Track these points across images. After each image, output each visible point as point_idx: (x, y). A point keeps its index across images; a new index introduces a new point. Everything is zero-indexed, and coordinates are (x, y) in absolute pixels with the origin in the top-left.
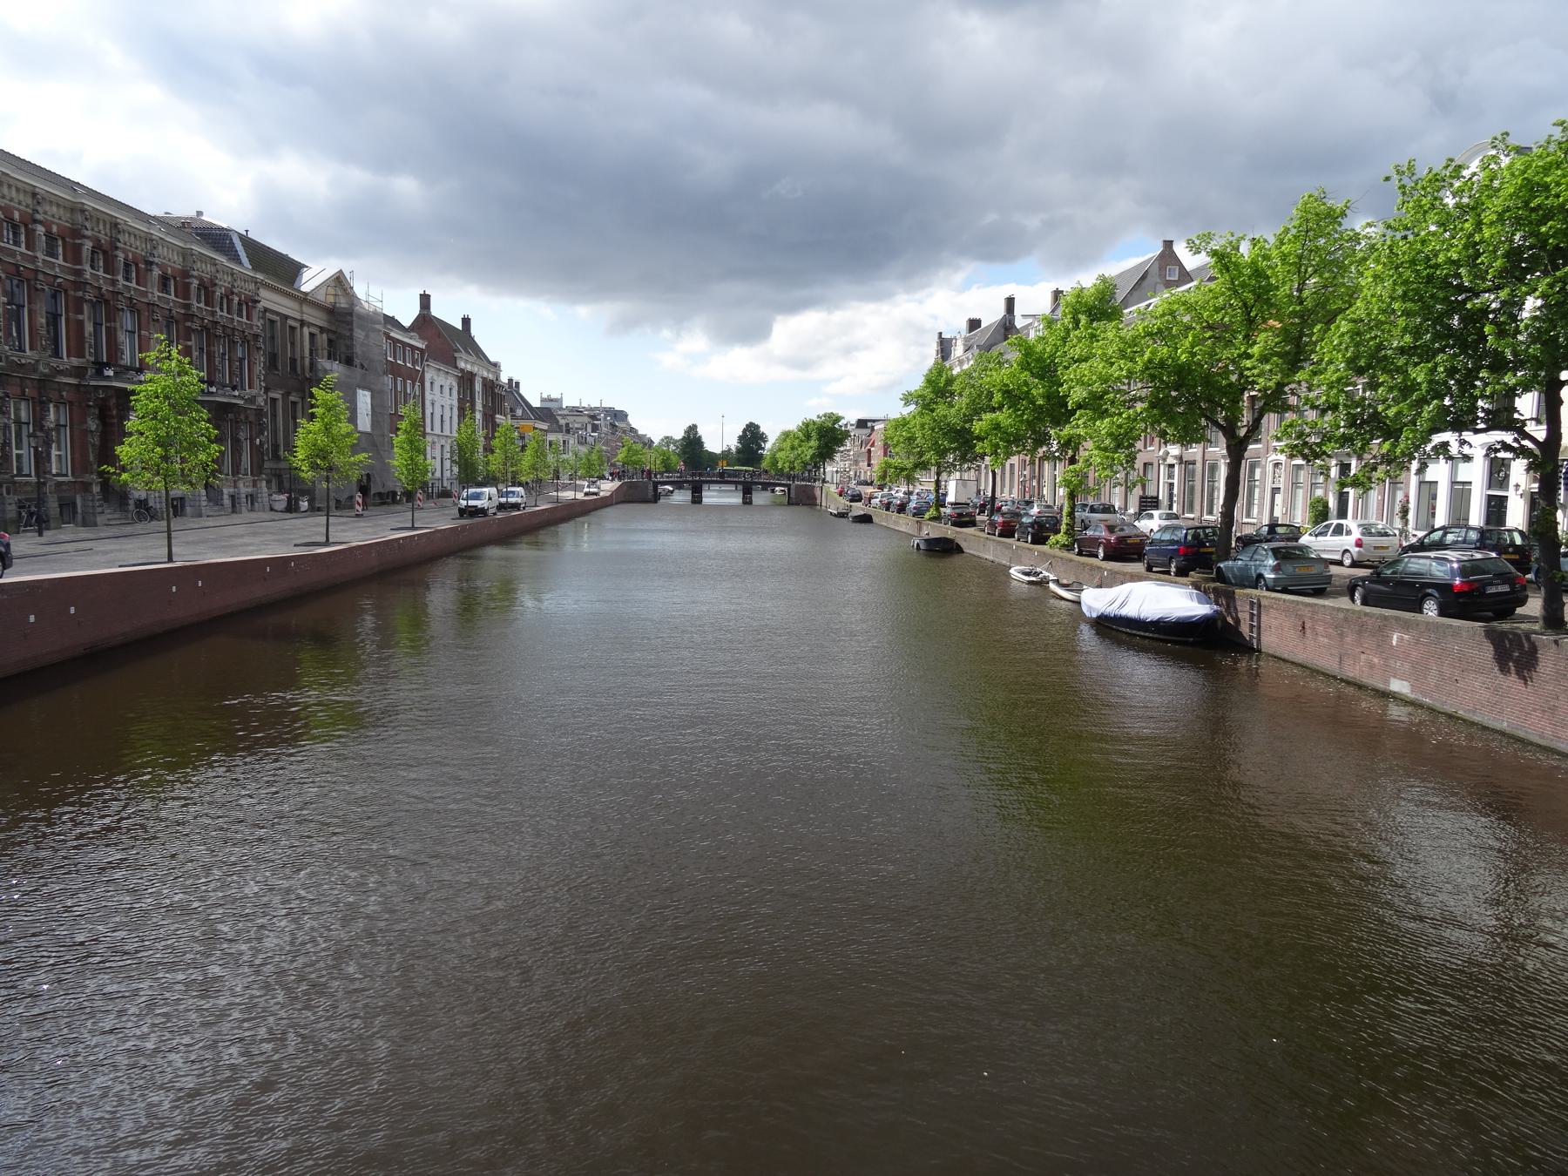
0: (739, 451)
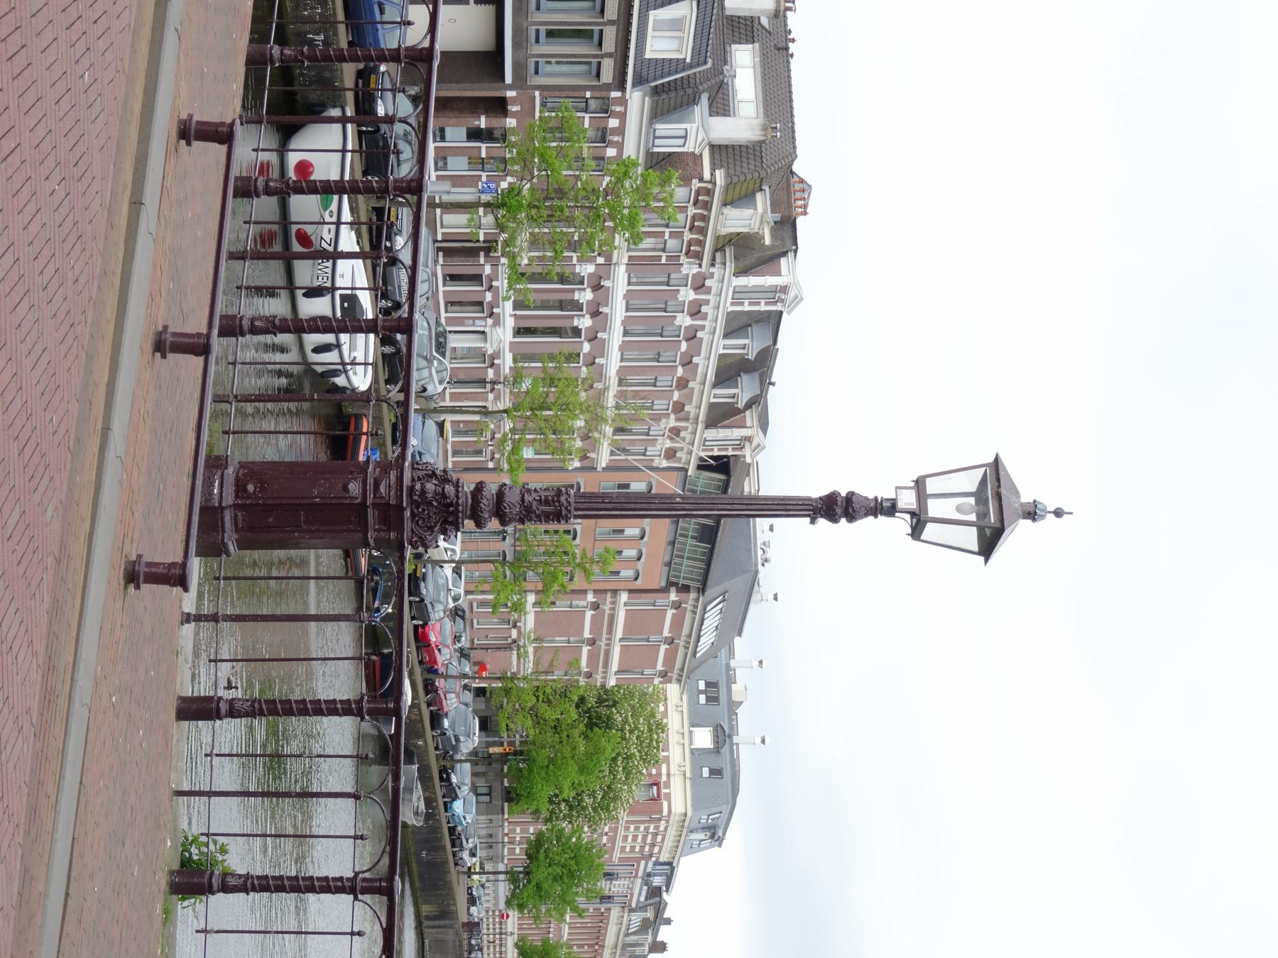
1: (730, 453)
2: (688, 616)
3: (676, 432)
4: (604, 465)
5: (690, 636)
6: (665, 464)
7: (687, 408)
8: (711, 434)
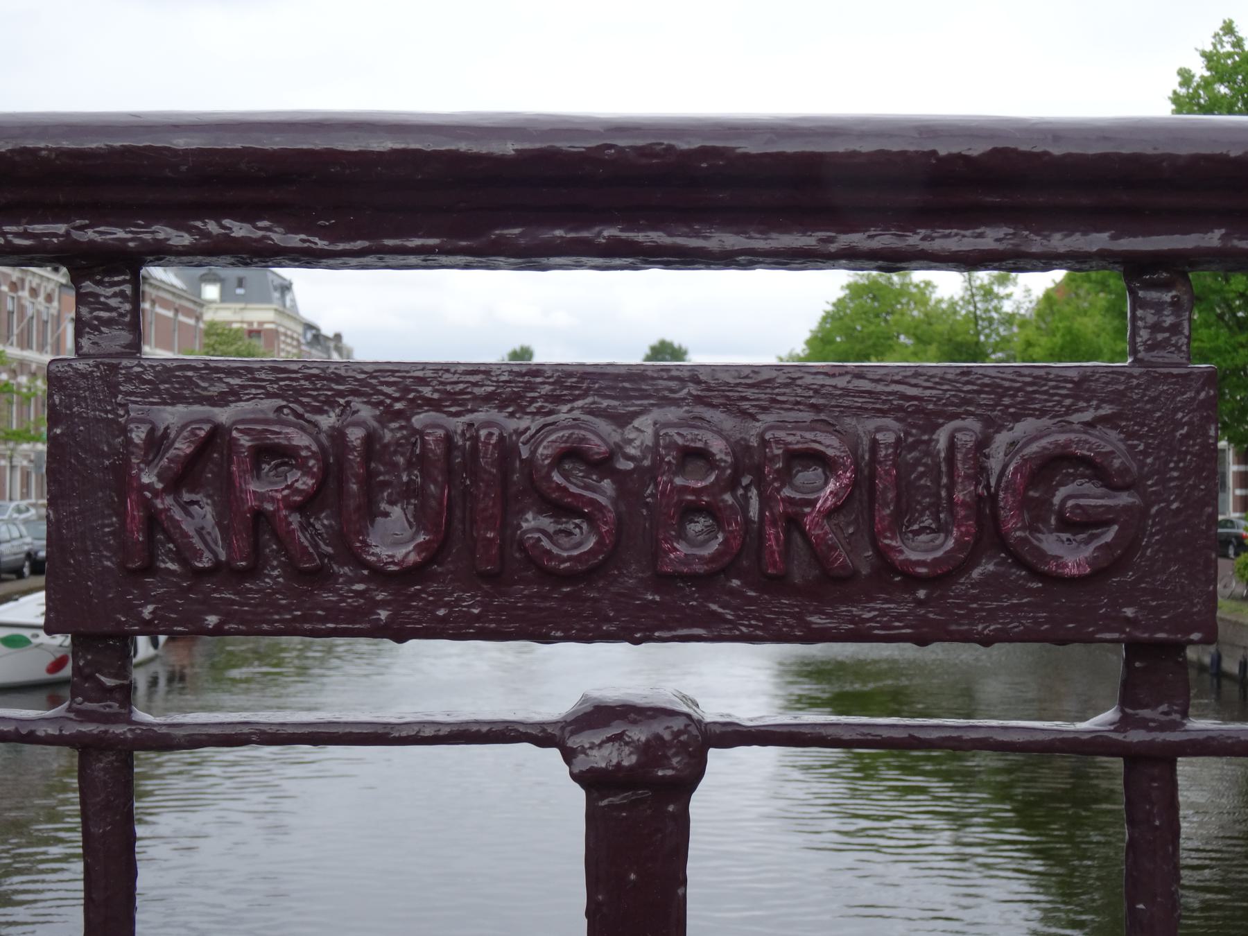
3: (34, 292)
5: (174, 294)
7: (14, 279)
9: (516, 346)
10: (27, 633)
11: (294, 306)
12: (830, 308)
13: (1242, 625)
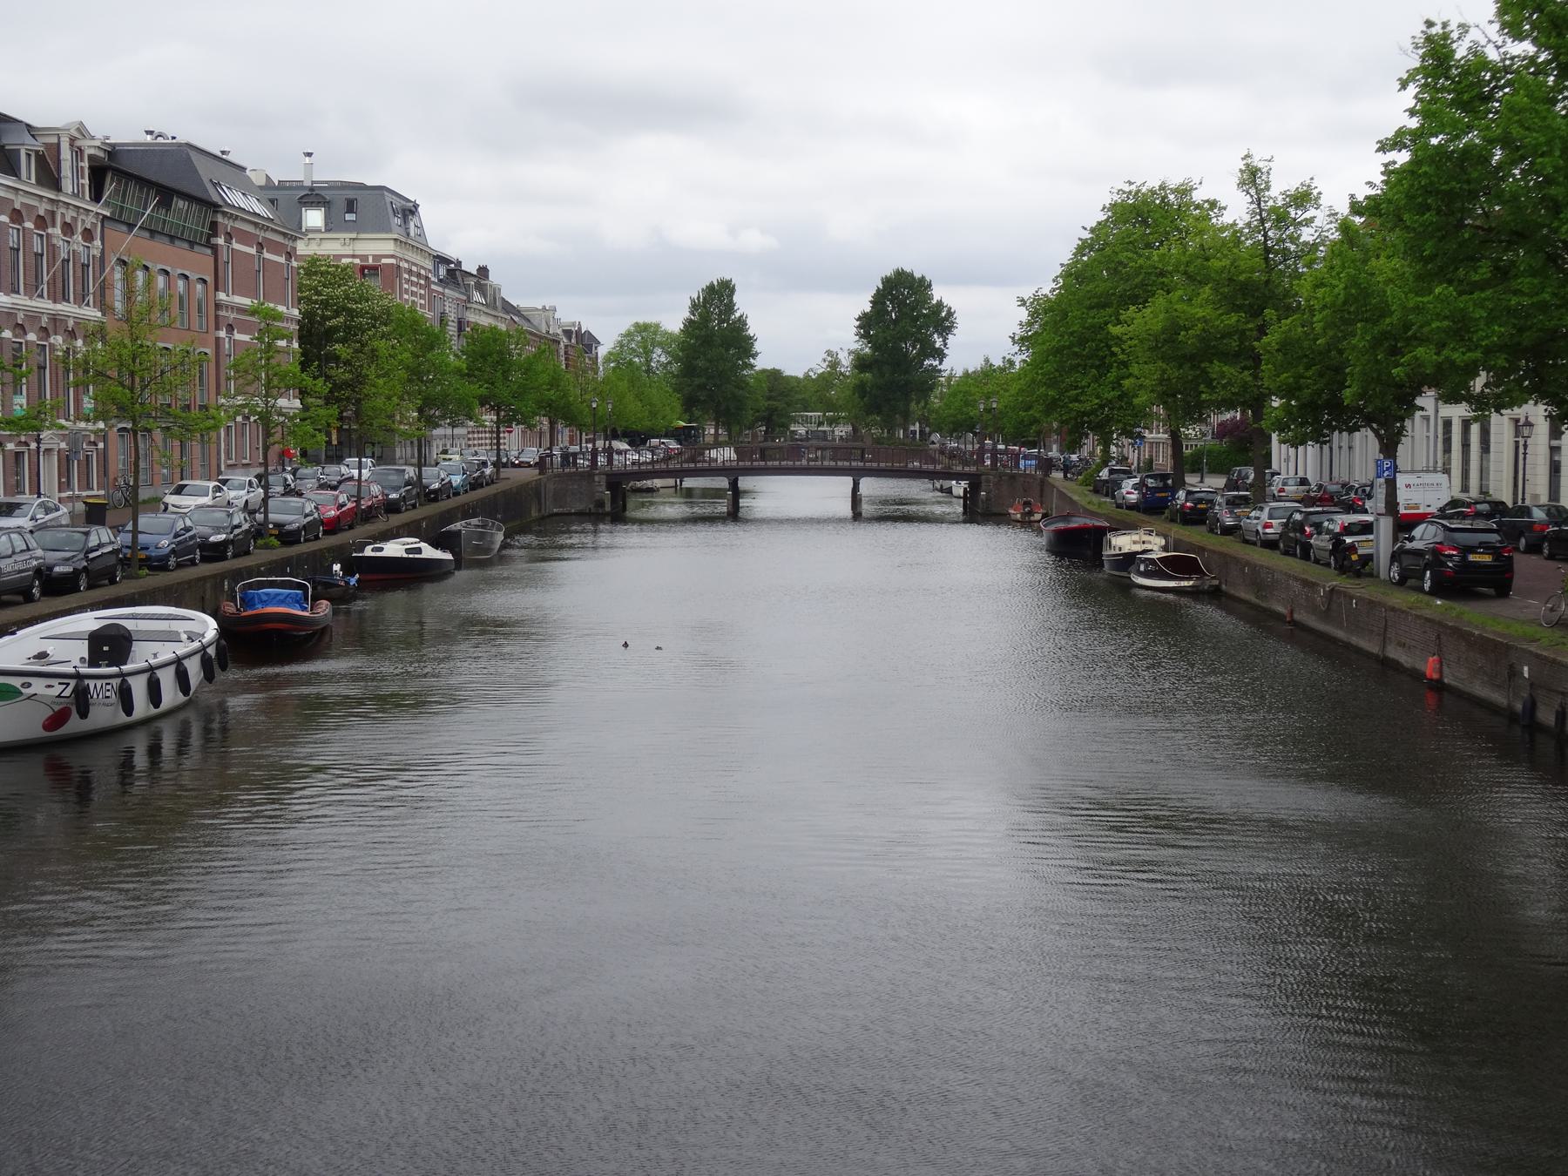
0: (861, 363)
1: (86, 164)
2: (239, 225)
3: (68, 229)
4: (99, 314)
5: (256, 224)
6: (98, 243)
7: (42, 213)
8: (67, 186)
9: (714, 278)
10: (16, 682)
11: (422, 235)
12: (1087, 235)
13: (1561, 664)
